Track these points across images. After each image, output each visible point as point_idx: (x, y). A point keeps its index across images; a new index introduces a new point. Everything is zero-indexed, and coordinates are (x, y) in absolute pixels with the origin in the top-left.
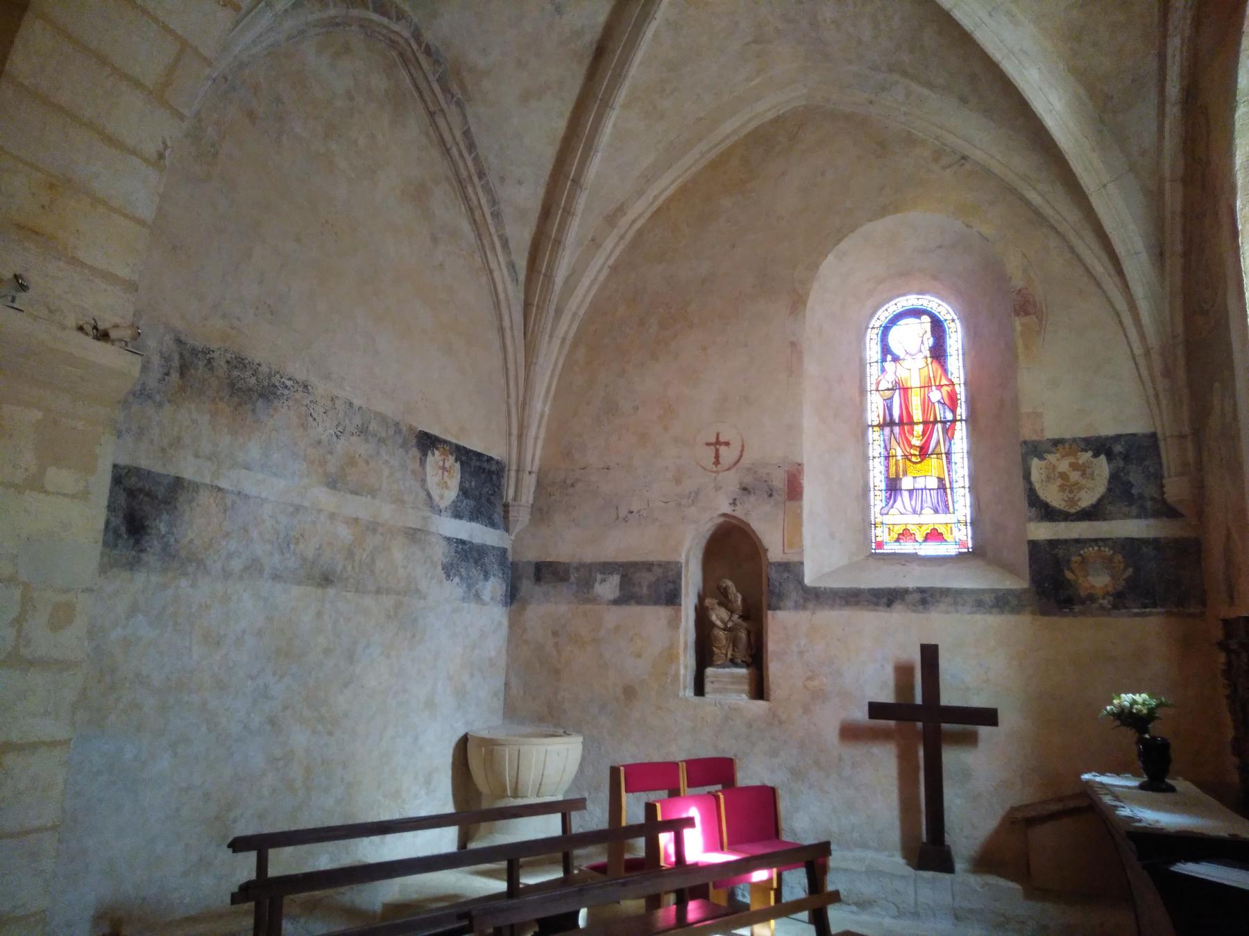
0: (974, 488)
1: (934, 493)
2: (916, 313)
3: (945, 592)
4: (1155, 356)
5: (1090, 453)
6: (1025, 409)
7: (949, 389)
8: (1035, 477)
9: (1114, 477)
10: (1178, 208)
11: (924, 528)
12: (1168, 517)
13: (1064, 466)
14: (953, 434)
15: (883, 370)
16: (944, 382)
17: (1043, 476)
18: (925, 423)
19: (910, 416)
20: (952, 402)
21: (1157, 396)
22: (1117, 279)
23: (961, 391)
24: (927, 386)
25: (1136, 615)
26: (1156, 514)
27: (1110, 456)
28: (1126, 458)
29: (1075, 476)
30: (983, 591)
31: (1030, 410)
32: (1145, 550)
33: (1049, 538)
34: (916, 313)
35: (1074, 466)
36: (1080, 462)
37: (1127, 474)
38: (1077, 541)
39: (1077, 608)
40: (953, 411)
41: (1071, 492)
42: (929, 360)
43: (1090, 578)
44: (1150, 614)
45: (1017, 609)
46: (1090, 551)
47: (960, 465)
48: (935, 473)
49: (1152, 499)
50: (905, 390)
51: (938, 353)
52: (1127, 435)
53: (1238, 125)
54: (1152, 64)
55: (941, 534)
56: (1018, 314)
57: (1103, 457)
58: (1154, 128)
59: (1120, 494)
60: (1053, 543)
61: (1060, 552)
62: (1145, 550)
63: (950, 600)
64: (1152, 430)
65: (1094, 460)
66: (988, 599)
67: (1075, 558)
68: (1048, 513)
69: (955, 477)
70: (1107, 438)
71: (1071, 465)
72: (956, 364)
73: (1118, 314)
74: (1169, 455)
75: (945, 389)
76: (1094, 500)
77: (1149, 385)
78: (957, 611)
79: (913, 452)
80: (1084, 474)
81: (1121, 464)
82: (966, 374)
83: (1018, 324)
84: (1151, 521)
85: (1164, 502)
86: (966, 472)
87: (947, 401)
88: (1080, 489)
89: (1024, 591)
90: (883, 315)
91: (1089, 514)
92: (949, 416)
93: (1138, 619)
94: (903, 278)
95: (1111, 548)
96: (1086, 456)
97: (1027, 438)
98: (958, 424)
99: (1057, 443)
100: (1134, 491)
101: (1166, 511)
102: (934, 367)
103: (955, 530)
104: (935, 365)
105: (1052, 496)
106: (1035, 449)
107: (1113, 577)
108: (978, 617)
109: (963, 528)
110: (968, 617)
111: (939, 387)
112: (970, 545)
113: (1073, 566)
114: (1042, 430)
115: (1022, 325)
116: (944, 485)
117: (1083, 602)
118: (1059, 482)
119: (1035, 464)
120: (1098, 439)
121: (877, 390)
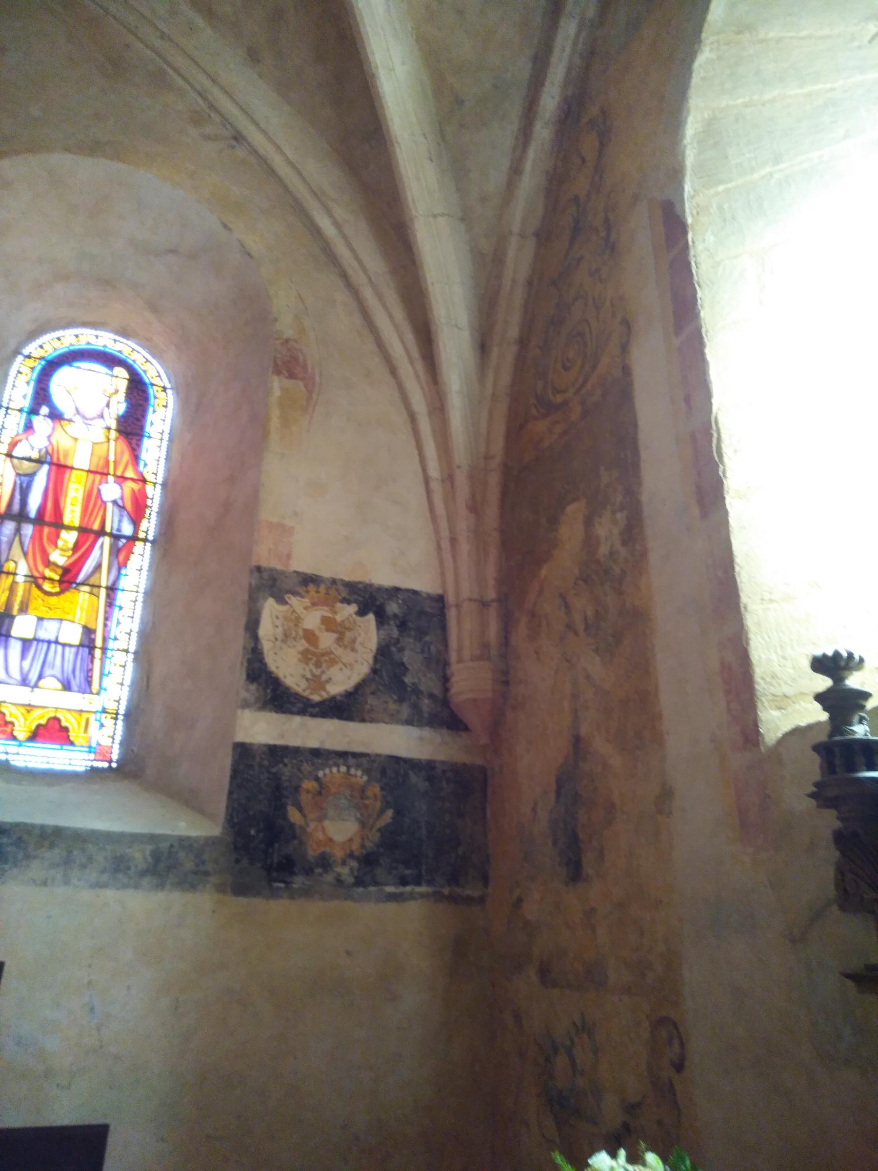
0: (144, 656)
1: (70, 653)
2: (109, 360)
3: (51, 836)
4: (461, 479)
5: (353, 608)
6: (266, 514)
7: (136, 486)
8: (266, 629)
9: (383, 652)
10: (523, 273)
11: (36, 713)
13: (312, 620)
14: (127, 558)
15: (29, 427)
16: (130, 473)
17: (280, 631)
18: (84, 531)
19: (58, 512)
20: (137, 509)
21: (453, 541)
22: (420, 366)
23: (154, 495)
24: (100, 472)
25: (392, 897)
26: (433, 721)
28: (403, 626)
29: (327, 640)
30: (135, 838)
31: (274, 520)
32: (413, 778)
33: (271, 742)
34: (109, 360)
35: (328, 624)
36: (339, 618)
37: (401, 650)
39: (299, 881)
41: (318, 665)
42: (113, 434)
43: (327, 823)
44: (412, 896)
45: (189, 882)
46: (333, 773)
47: (127, 611)
48: (81, 617)
49: (431, 696)
50: (60, 470)
51: (131, 428)
52: (407, 590)
53: (695, 80)
54: (522, 69)
55: (66, 730)
56: (278, 372)
57: (371, 617)
58: (505, 164)
59: (387, 685)
60: (277, 753)
61: (286, 771)
62: (413, 778)
63: (56, 854)
65: (358, 619)
66: (139, 856)
67: (309, 785)
68: (278, 698)
69: (114, 631)
70: (380, 589)
72: (154, 454)
73: (412, 417)
74: (464, 632)
75: (129, 485)
77: (444, 525)
78: (67, 882)
79: (48, 573)
80: (340, 640)
81: (395, 633)
82: (168, 470)
83: (277, 385)
85: (445, 702)
86: (135, 626)
87: (128, 505)
88: (333, 662)
89: (210, 842)
90: (51, 344)
91: (341, 708)
92: (127, 529)
93: (392, 906)
94: (96, 290)
95: (367, 772)
97: (264, 564)
98: (139, 545)
99: (308, 580)
100: (407, 680)
101: (447, 718)
102: (115, 448)
103: (94, 725)
104: (122, 445)
106: (271, 584)
107: (363, 824)
108: (110, 894)
109: (108, 721)
110: (86, 895)
111: (121, 479)
112: (115, 756)
113: (304, 798)
114: (289, 556)
115: (282, 389)
116: (93, 641)
117: (308, 871)
118: (303, 645)
119: (270, 608)
121: (9, 455)
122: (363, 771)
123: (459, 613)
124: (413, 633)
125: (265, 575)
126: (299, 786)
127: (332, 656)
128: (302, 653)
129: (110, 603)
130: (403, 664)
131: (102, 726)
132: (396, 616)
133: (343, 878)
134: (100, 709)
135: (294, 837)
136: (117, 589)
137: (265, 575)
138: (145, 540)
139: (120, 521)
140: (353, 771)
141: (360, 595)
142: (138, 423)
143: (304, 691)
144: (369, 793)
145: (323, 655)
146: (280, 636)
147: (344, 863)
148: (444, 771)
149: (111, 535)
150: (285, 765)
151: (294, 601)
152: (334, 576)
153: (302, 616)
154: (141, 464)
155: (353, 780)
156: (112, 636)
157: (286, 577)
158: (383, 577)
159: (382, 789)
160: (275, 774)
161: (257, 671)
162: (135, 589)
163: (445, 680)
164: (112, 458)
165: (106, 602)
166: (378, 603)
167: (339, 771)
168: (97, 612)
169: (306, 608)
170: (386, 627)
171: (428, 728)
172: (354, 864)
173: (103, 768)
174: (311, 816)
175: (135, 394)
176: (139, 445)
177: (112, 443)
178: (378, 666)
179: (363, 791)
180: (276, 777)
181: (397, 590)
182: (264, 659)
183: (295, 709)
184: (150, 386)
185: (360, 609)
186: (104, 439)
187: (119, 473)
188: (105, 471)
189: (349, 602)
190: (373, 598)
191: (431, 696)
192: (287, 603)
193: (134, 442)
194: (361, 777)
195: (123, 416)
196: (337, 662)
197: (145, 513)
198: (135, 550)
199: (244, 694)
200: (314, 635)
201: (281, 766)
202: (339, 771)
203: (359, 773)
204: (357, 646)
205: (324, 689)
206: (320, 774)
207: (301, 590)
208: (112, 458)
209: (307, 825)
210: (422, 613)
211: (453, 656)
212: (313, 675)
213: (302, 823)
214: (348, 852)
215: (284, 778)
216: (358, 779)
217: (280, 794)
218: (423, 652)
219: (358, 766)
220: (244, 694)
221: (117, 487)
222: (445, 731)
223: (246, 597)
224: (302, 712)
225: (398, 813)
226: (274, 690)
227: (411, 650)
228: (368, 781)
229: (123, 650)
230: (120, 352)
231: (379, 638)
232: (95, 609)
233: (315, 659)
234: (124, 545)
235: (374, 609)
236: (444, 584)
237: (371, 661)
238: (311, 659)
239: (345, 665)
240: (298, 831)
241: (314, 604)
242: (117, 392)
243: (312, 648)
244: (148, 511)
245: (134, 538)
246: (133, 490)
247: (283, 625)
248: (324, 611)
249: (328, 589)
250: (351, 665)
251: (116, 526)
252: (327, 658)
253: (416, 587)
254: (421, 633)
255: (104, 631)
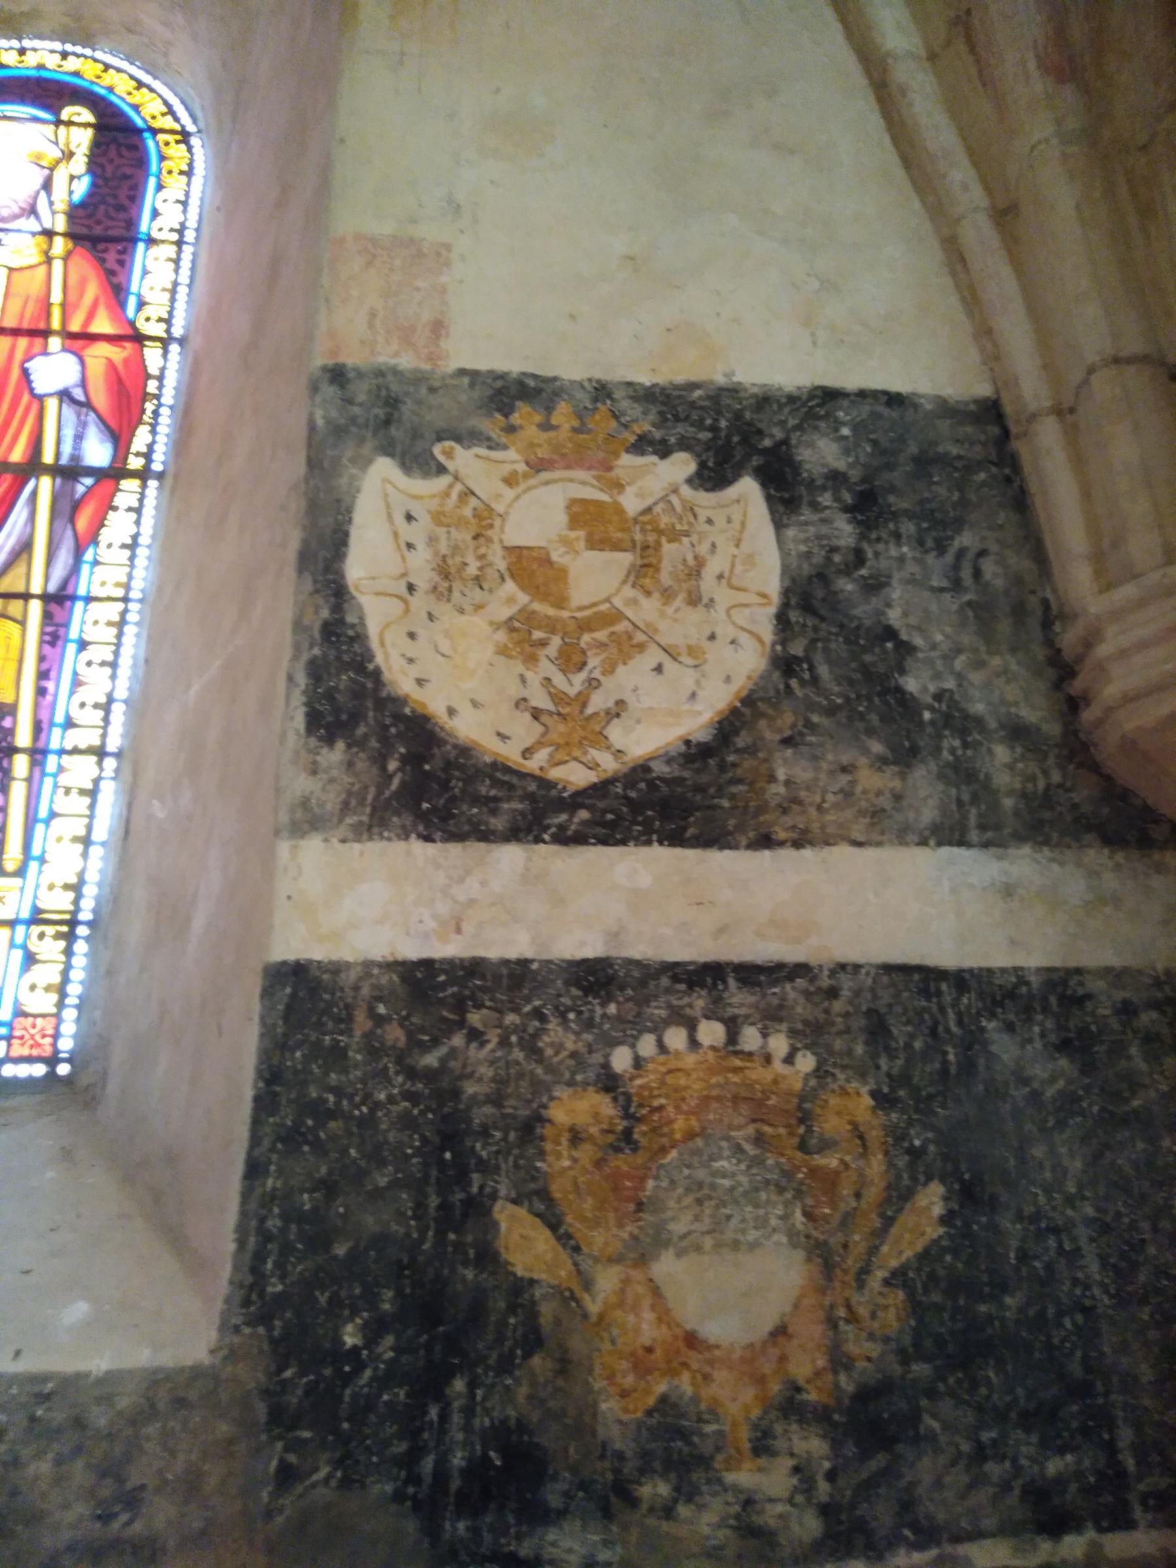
5: (682, 465)
8: (368, 562)
9: (806, 600)
12: (1111, 839)
14: (99, 523)
16: (103, 325)
17: (421, 563)
26: (1041, 823)
27: (785, 487)
28: (867, 506)
29: (595, 577)
32: (1004, 1048)
33: (411, 951)
34: (48, 94)
35: (594, 523)
36: (631, 503)
37: (875, 586)
38: (595, 978)
40: (120, 438)
41: (571, 660)
42: (60, 245)
43: (665, 1266)
46: (674, 1054)
49: (1017, 732)
51: (104, 227)
57: (748, 487)
59: (837, 704)
60: (436, 991)
61: (480, 1063)
62: (1004, 1048)
64: (984, 390)
65: (704, 499)
67: (576, 1108)
68: (431, 787)
70: (765, 400)
71: (582, 515)
76: (697, 721)
80: (644, 571)
81: (844, 531)
84: (1023, 865)
85: (1077, 749)
87: (100, 399)
88: (626, 647)
92: (98, 453)
95: (809, 1034)
96: (659, 480)
97: (352, 358)
99: (509, 395)
102: (65, 277)
104: (83, 265)
105: (460, 679)
107: (824, 1258)
109: (50, 948)
111: (80, 340)
113: (562, 1164)
114: (438, 327)
117: (612, 1499)
118: (509, 599)
119: (380, 491)
120: (722, 398)
122: (793, 1033)
123: (1072, 435)
124: (908, 528)
125: (361, 391)
126: (538, 1119)
127: (621, 627)
128: (509, 625)
129: (53, 636)
130: (890, 633)
131: (30, 959)
132: (836, 478)
133: (770, 1515)
134: (25, 914)
135: (533, 1341)
136: (73, 598)
137: (361, 391)
138: (143, 475)
139: (79, 438)
140: (750, 1038)
141: (699, 425)
142: (122, 215)
143: (527, 753)
144: (831, 1125)
145: (585, 626)
146: (424, 578)
147: (762, 1446)
148: (1127, 1010)
149: (56, 470)
150: (475, 1035)
151: (465, 460)
152: (599, 374)
153: (499, 508)
154: (132, 302)
155: (759, 1074)
156: (59, 718)
157: (432, 390)
158: (772, 358)
159: (883, 1101)
160: (430, 1075)
161: (346, 697)
162: (120, 593)
163: (1063, 672)
164: (56, 297)
165: (43, 633)
166: (767, 443)
167: (694, 1043)
168: (20, 662)
169: (510, 480)
170: (807, 514)
171: (1026, 850)
172: (812, 1445)
173: (31, 1080)
174: (597, 1239)
175: (113, 153)
176: (125, 261)
177: (58, 266)
178: (797, 648)
179: (805, 1118)
180: (443, 1090)
181: (829, 396)
182: (369, 656)
183: (498, 823)
184: (147, 135)
185: (702, 465)
186: (36, 258)
187: (75, 326)
188: (42, 326)
189: (664, 451)
190: (749, 433)
191: (1017, 732)
192: (441, 470)
193: (111, 257)
194: (789, 1060)
195: (83, 205)
196: (641, 647)
197: (143, 411)
198: (120, 500)
199: (302, 784)
200: (549, 562)
201: (458, 1040)
202: (694, 1043)
203: (779, 1044)
204: (708, 584)
205: (601, 740)
206: (621, 1060)
207: (491, 425)
208: (56, 297)
209: (588, 1284)
210: (925, 463)
211: (1078, 580)
212: (558, 697)
213: (564, 1272)
214: (775, 1387)
215: (470, 1089)
216: (778, 1066)
217: (461, 1156)
218: (956, 585)
219: (770, 1017)
220: (302, 784)
221: (71, 360)
222: (1097, 856)
223: (298, 466)
224: (527, 830)
225: (969, 1196)
226: (413, 760)
227: (912, 581)
228: (821, 1073)
229: (90, 751)
230: (76, 74)
231: (784, 553)
232: (14, 654)
233: (556, 641)
234: (90, 489)
235: (756, 461)
236: (993, 355)
237: (767, 632)
238: (543, 643)
239: (671, 653)
240: (547, 1311)
241: (537, 466)
242: (69, 155)
243: (544, 609)
244: (149, 407)
245: (115, 473)
246: (110, 363)
247: (432, 540)
248: (583, 486)
249: (581, 414)
250: (692, 651)
251: (67, 449)
252: (601, 635)
253: (898, 384)
254: (937, 528)
255: (37, 706)
